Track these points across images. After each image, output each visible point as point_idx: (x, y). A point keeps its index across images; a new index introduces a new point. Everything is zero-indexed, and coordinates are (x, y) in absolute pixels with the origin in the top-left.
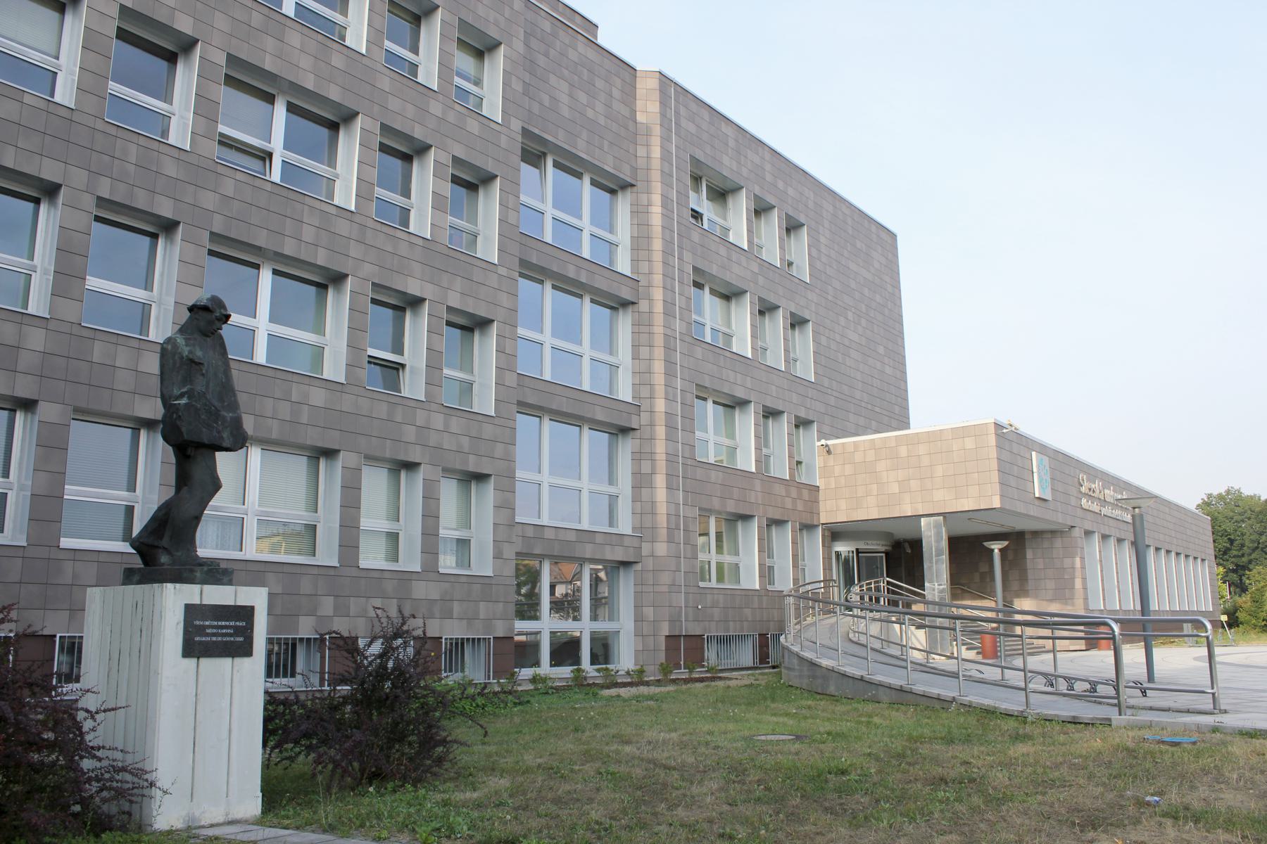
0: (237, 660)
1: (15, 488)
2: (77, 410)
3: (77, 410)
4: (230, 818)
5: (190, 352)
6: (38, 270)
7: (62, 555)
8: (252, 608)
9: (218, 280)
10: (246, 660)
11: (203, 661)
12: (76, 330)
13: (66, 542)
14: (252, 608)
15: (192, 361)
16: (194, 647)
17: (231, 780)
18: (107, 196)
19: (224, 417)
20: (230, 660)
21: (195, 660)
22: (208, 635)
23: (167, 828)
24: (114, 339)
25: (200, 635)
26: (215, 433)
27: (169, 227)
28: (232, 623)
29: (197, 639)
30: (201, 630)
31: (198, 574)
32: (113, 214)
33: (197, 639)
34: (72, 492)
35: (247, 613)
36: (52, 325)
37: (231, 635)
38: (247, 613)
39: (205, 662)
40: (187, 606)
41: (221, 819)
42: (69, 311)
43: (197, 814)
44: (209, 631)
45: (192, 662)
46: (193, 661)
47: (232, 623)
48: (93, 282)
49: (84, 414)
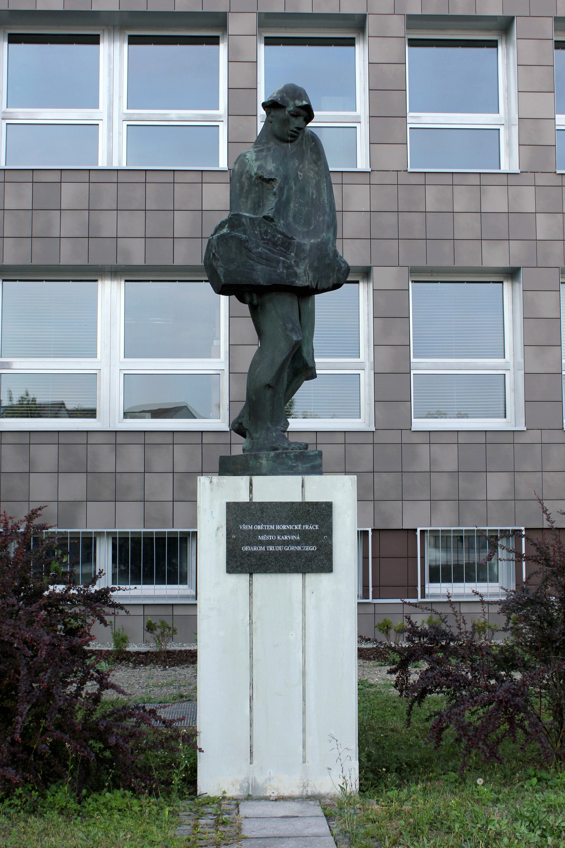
0: (311, 578)
1: (512, 369)
2: (414, 271)
3: (414, 271)
4: (310, 791)
5: (260, 168)
6: (362, 121)
7: (416, 439)
8: (329, 505)
9: (299, 66)
10: (324, 577)
11: (258, 578)
12: (403, 178)
13: (418, 424)
14: (329, 505)
15: (261, 178)
16: (243, 560)
17: (309, 740)
18: (418, 12)
19: (300, 247)
20: (297, 578)
21: (246, 577)
22: (261, 543)
23: (219, 794)
24: (448, 180)
25: (250, 544)
26: (280, 269)
27: (505, 26)
28: (298, 527)
29: (246, 548)
30: (252, 538)
31: (264, 462)
32: (431, 32)
33: (246, 548)
34: (421, 366)
35: (322, 513)
36: (375, 178)
37: (297, 543)
38: (322, 513)
39: (260, 579)
40: (229, 505)
41: (296, 792)
42: (390, 158)
43: (260, 780)
44: (263, 538)
45: (241, 580)
46: (244, 578)
47: (298, 527)
48: (417, 119)
49: (423, 274)
